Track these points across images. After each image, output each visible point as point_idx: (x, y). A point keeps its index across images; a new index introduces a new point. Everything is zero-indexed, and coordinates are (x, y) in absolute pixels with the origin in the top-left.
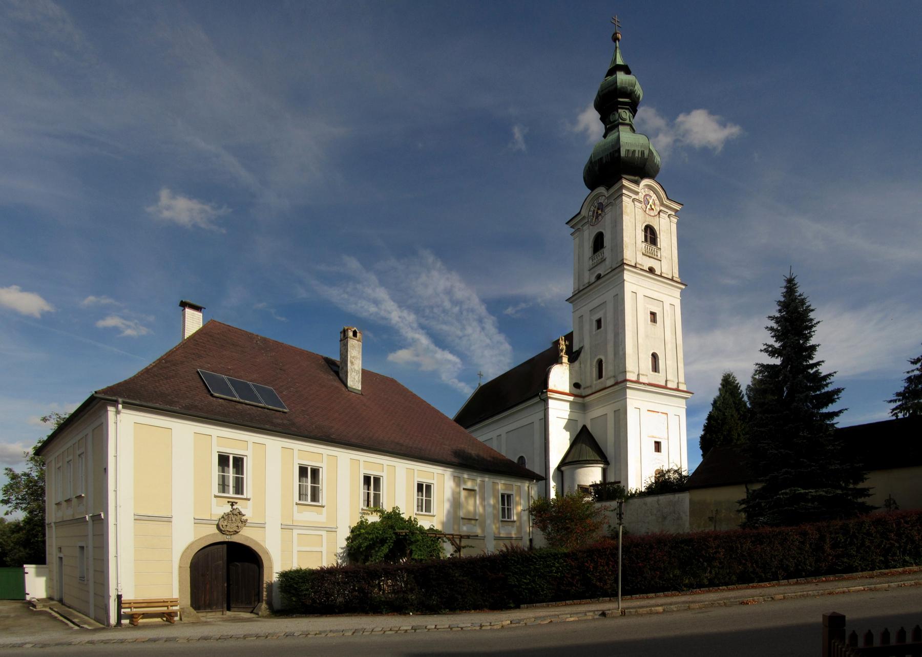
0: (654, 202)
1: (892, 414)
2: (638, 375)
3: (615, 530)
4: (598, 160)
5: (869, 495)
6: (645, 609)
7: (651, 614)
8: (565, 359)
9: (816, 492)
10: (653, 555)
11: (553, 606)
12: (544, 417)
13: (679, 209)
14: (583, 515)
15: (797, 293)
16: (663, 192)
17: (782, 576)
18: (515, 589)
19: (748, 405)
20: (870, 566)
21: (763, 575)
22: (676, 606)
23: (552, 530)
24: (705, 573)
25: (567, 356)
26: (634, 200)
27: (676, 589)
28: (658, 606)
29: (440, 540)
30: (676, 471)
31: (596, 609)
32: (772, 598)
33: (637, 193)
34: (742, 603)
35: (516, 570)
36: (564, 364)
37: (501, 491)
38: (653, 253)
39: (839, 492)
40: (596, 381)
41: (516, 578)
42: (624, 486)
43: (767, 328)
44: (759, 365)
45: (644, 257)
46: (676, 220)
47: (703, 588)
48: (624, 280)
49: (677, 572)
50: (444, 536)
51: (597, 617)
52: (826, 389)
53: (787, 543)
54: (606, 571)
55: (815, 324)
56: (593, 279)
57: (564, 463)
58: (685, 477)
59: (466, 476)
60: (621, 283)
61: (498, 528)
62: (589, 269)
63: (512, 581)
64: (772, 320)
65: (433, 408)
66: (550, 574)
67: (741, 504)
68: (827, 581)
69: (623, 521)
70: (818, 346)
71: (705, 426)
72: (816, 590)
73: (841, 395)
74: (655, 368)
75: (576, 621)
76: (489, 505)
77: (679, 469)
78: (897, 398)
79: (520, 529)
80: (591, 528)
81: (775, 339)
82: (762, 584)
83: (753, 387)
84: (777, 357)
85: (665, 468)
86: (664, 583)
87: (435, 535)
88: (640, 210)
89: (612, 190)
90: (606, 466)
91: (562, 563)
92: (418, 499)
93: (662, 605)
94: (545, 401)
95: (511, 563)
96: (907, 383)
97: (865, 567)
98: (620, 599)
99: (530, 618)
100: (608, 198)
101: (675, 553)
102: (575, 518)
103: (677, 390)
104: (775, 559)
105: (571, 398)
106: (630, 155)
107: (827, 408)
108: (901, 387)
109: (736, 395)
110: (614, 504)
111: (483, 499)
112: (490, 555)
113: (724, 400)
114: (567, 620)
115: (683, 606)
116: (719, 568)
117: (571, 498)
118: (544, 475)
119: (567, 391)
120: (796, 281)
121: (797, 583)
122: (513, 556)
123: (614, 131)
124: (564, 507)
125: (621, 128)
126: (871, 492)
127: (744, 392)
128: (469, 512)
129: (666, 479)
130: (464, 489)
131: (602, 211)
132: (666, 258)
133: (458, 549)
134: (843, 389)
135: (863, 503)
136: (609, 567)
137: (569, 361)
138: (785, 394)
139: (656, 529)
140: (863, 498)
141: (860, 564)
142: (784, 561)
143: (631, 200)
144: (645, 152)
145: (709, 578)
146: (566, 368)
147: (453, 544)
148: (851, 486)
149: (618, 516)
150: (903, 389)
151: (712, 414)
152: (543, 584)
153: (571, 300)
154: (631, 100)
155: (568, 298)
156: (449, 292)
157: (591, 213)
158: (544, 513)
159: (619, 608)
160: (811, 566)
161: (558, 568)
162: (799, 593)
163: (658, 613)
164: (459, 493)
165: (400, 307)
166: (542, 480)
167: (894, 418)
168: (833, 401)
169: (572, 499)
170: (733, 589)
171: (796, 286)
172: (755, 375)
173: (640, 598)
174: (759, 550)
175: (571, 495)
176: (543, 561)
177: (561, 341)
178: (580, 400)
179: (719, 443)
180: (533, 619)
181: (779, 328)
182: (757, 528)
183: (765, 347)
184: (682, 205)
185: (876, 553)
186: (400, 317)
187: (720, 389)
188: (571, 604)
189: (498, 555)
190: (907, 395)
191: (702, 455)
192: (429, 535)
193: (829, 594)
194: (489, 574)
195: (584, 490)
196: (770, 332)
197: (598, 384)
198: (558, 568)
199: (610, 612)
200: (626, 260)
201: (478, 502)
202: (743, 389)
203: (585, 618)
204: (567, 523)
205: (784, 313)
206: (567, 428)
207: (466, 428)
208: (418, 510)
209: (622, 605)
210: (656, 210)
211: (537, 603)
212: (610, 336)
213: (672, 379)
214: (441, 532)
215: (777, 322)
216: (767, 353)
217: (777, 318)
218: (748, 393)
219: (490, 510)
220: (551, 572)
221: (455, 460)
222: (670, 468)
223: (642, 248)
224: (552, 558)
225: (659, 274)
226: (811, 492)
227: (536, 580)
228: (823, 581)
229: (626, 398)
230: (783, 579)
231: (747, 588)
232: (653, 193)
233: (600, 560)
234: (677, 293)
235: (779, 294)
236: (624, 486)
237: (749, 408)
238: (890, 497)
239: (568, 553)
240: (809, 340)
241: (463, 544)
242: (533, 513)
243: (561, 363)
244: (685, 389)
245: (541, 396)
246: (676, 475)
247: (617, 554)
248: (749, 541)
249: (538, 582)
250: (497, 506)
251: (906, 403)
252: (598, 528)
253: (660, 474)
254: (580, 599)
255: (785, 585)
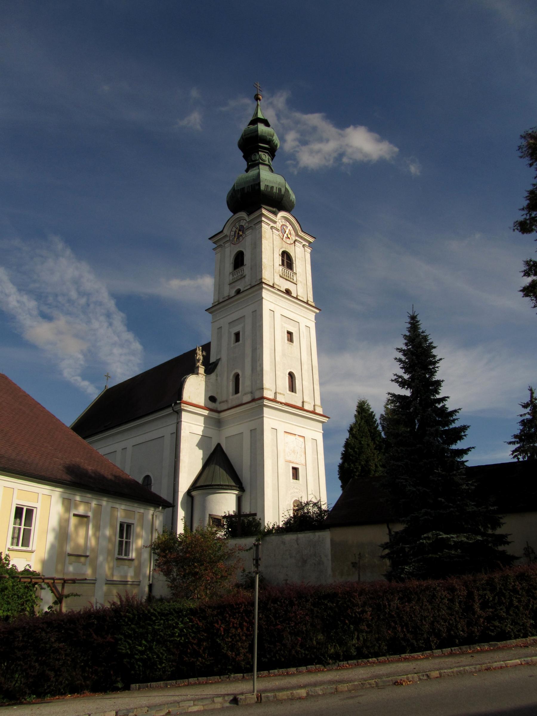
0: (290, 232)
1: (513, 456)
2: (276, 393)
3: (250, 575)
4: (241, 189)
5: (508, 543)
6: (285, 693)
7: (292, 699)
8: (202, 370)
9: (457, 537)
10: (293, 614)
11: (173, 686)
12: (175, 431)
13: (312, 241)
14: (214, 557)
15: (420, 329)
16: (298, 225)
17: (435, 644)
18: (125, 660)
19: (383, 434)
20: (523, 631)
21: (415, 643)
22: (322, 687)
23: (177, 575)
24: (352, 639)
25: (204, 367)
26: (272, 228)
27: (320, 662)
28: (300, 687)
29: (36, 586)
30: (315, 504)
31: (226, 693)
32: (427, 675)
33: (275, 222)
34: (397, 683)
35: (130, 632)
36: (200, 375)
37: (120, 520)
38: (290, 277)
39: (479, 538)
40: (232, 395)
41: (129, 644)
42: (260, 519)
43: (396, 359)
44: (391, 394)
45: (281, 279)
46: (310, 251)
47: (352, 659)
48: (262, 298)
49: (320, 637)
50: (42, 581)
51: (228, 704)
52: (453, 426)
53: (436, 601)
54: (239, 635)
55: (438, 360)
56: (233, 293)
57: (195, 486)
58: (325, 511)
59: (78, 498)
60: (259, 300)
61: (112, 569)
62: (229, 283)
63: (124, 648)
64: (400, 352)
65: (48, 412)
66: (172, 639)
67: (384, 549)
68: (482, 651)
69: (260, 569)
70: (443, 381)
71: (342, 454)
72: (472, 665)
73: (467, 432)
74: (292, 388)
75: (200, 711)
76: (104, 536)
77: (318, 503)
78: (515, 440)
79: (138, 571)
80: (223, 574)
81: (403, 371)
82: (415, 655)
83: (386, 416)
84: (407, 388)
85: (304, 500)
86: (307, 652)
87: (29, 580)
88: (277, 237)
89: (252, 216)
90: (241, 493)
91: (187, 623)
92: (14, 528)
93: (304, 687)
94: (178, 413)
95: (124, 621)
96: (522, 426)
97: (517, 633)
98: (256, 677)
99: (141, 707)
100: (249, 222)
101: (318, 612)
102: (206, 561)
103: (313, 412)
104: (425, 621)
105: (206, 413)
106: (269, 190)
107: (456, 445)
108: (517, 429)
109: (371, 423)
110: (250, 541)
111: (97, 528)
112: (98, 608)
113: (360, 428)
114: (190, 710)
115: (329, 687)
116: (366, 632)
117: (201, 535)
118: (170, 500)
119: (202, 404)
120: (418, 318)
121: (451, 654)
122: (128, 611)
123: (255, 168)
124: (193, 546)
125: (261, 166)
126: (509, 539)
127: (378, 421)
128: (77, 546)
129: (305, 513)
130: (75, 515)
131: (243, 233)
132: (301, 282)
133: (59, 600)
134: (468, 427)
135: (504, 552)
136: (242, 629)
137: (206, 372)
138: (417, 427)
139: (295, 579)
140: (503, 546)
141: (512, 629)
142: (435, 624)
143: (270, 227)
144: (282, 189)
145: (357, 646)
146: (202, 379)
147: (53, 592)
148: (490, 532)
149: (255, 561)
150: (519, 431)
151: (349, 442)
152: (161, 653)
153: (210, 311)
154: (270, 146)
155: (207, 308)
156: (77, 282)
157: (233, 233)
158: (170, 551)
159: (254, 692)
160: (463, 631)
161: (181, 630)
162: (456, 669)
163: (300, 698)
164: (68, 521)
165: (20, 290)
166: (169, 507)
167: (515, 460)
168: (460, 438)
169: (203, 535)
170: (384, 663)
171: (419, 323)
172: (387, 405)
173: (279, 675)
174: (408, 610)
175: (202, 530)
176: (164, 620)
177: (198, 351)
178: (215, 415)
179: (357, 474)
180: (146, 709)
181: (407, 361)
182: (403, 580)
183: (396, 377)
184: (315, 238)
185: (526, 615)
186: (18, 302)
187: (355, 416)
188: (195, 684)
189: (109, 610)
190: (523, 437)
191: (342, 486)
192: (22, 580)
193: (487, 670)
194: (95, 636)
195: (217, 521)
196: (399, 363)
197: (234, 399)
198: (181, 630)
199: (243, 697)
200: (265, 279)
201: (90, 532)
202: (377, 417)
203: (212, 707)
204: (195, 567)
205: (410, 347)
206: (200, 445)
207: (84, 438)
208: (12, 544)
209: (259, 685)
210: (292, 239)
211: (152, 682)
212: (248, 351)
213: (308, 400)
214: (39, 575)
215: (404, 355)
216: (398, 383)
217: (404, 350)
218: (382, 422)
219: (104, 543)
220: (173, 635)
221: (67, 477)
222: (309, 500)
223: (279, 271)
224: (175, 615)
225: (295, 297)
226: (453, 538)
227: (154, 647)
228: (478, 652)
229: (263, 417)
230: (437, 648)
231: (399, 661)
232: (289, 224)
233: (233, 620)
234: (312, 316)
235: (404, 326)
236: (260, 519)
237: (383, 438)
238: (528, 545)
239: (196, 609)
240: (434, 375)
241: (66, 592)
242: (157, 551)
243: (198, 374)
244: (321, 413)
245: (174, 408)
246: (316, 509)
247: (252, 612)
248: (397, 598)
249: (156, 651)
250: (113, 538)
251: (523, 446)
252: (231, 574)
253: (299, 507)
254: (207, 676)
255: (439, 657)
